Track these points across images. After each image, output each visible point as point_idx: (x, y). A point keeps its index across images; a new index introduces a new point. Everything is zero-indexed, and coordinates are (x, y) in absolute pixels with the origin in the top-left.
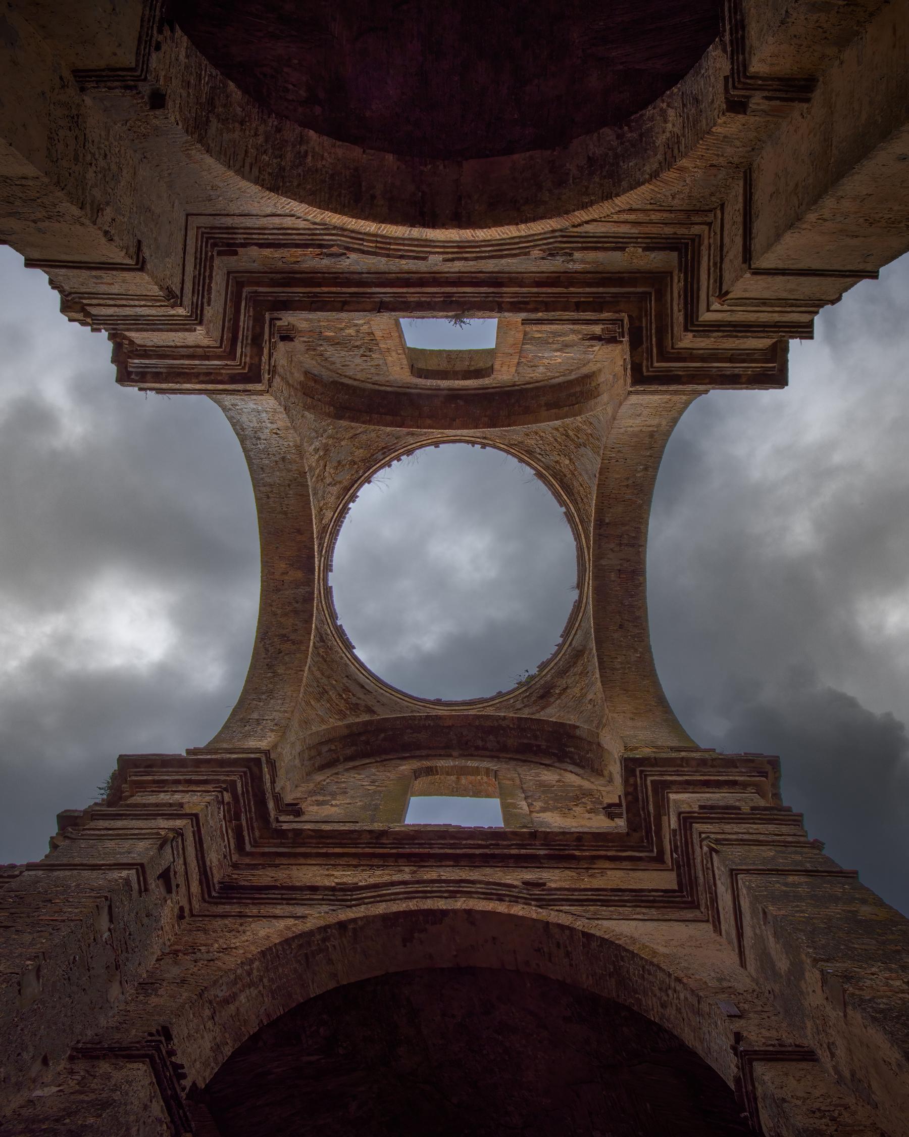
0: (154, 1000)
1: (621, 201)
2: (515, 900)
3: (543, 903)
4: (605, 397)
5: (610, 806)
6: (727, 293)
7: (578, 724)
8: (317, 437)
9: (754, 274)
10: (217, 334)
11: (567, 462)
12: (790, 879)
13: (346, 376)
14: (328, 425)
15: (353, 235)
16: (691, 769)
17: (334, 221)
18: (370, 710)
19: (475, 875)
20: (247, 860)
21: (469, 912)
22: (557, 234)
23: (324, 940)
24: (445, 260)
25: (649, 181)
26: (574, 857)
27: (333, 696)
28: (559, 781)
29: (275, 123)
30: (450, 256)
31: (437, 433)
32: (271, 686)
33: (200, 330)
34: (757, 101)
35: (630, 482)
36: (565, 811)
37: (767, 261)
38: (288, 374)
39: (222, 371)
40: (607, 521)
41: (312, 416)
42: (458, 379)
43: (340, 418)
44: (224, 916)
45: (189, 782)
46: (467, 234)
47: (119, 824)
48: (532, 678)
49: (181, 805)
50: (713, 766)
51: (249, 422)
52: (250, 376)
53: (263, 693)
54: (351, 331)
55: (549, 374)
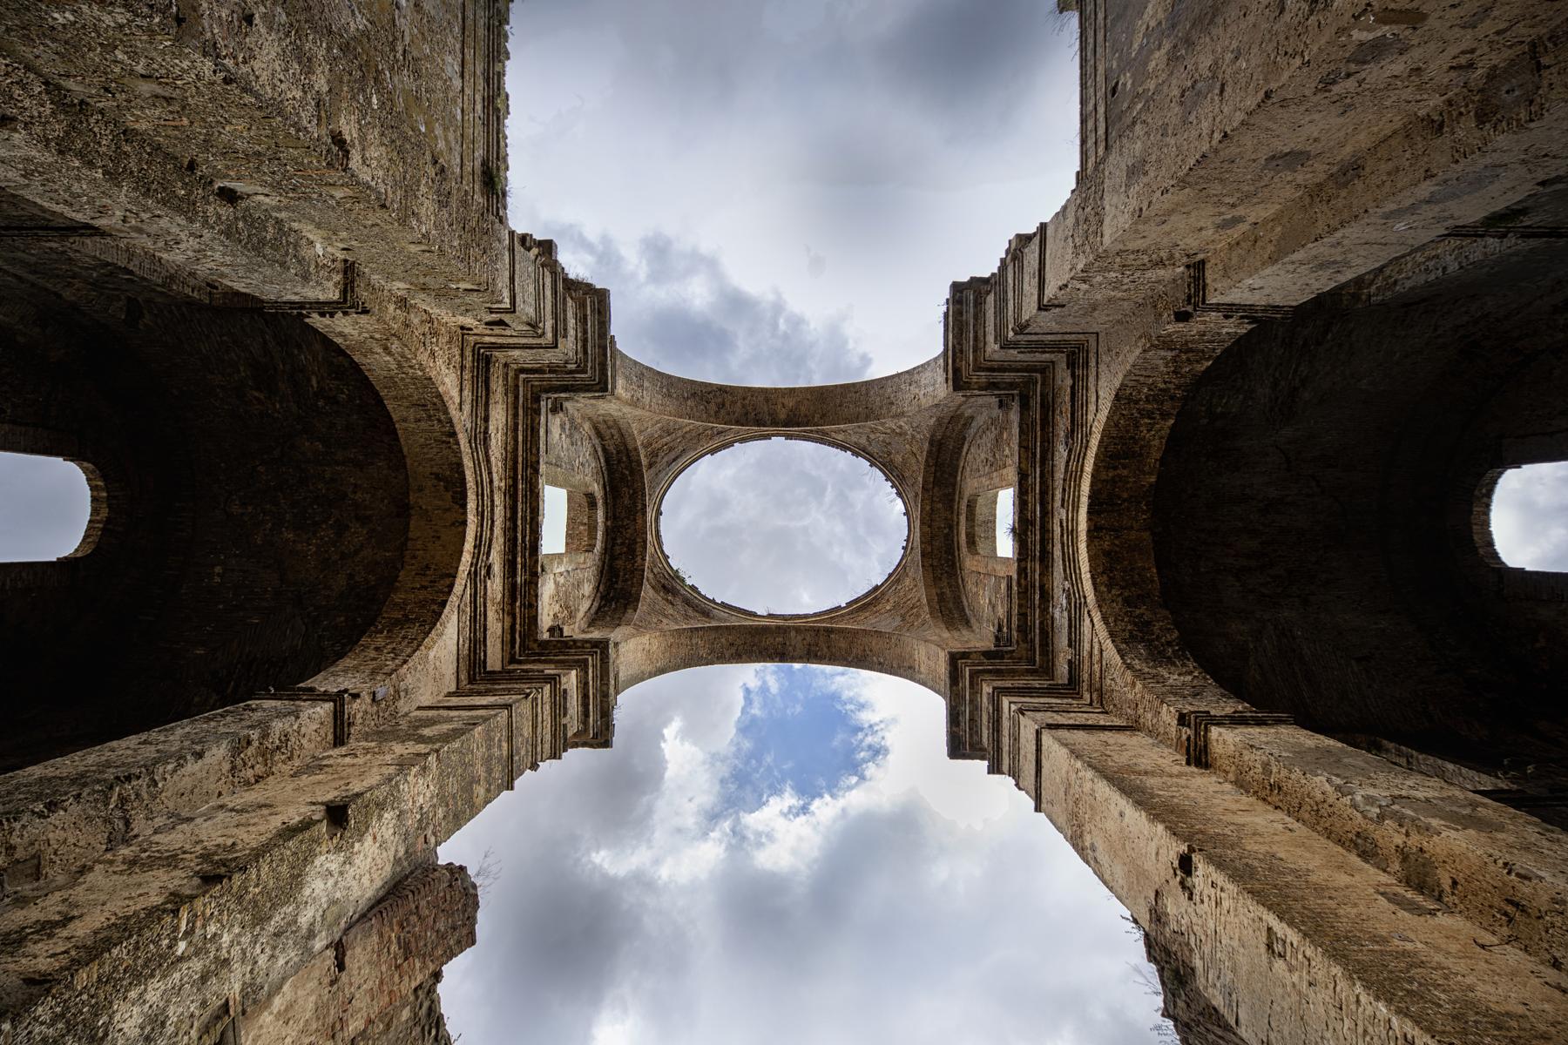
0: (392, 307)
1: (1109, 645)
2: (476, 556)
3: (473, 575)
4: (946, 634)
5: (561, 630)
10: (996, 357)
12: (505, 745)
18: (650, 466)
19: (498, 531)
20: (511, 374)
21: (464, 523)
23: (439, 421)
25: (1124, 662)
26: (513, 599)
31: (917, 514)
33: (997, 347)
34: (1187, 732)
36: (556, 597)
37: (1046, 738)
43: (931, 444)
44: (462, 355)
45: (585, 341)
46: (1083, 537)
47: (548, 293)
48: (683, 580)
49: (565, 336)
51: (926, 378)
52: (958, 382)
54: (1007, 452)
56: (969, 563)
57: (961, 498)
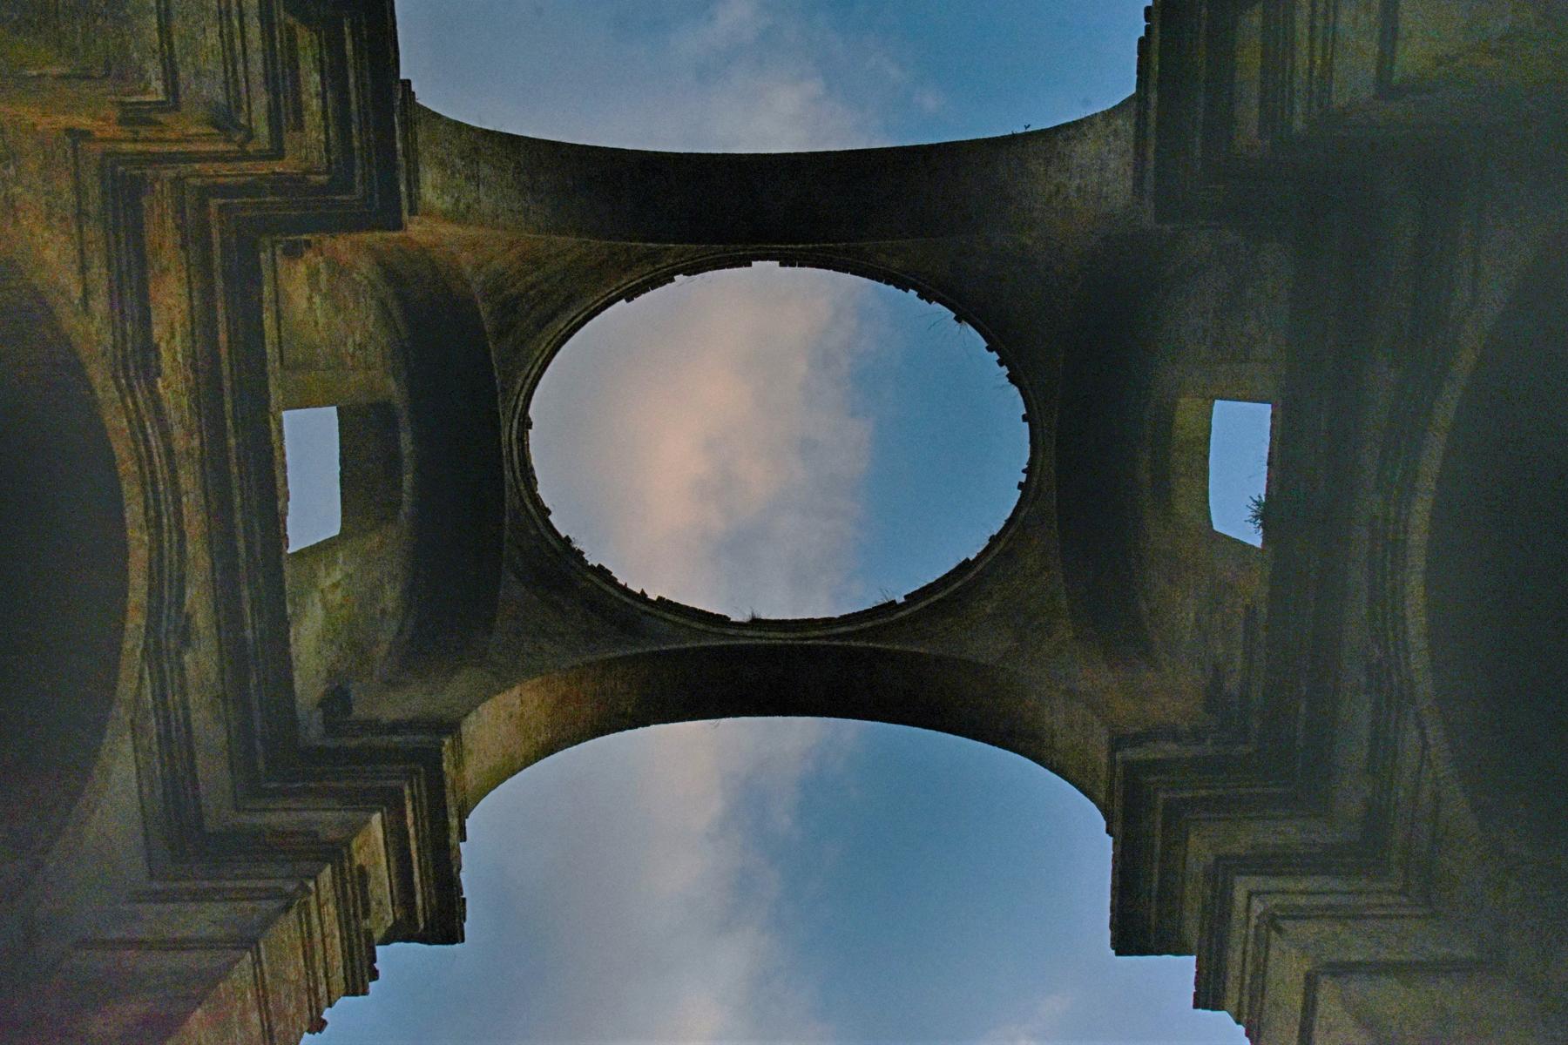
3: (154, 653)
6: (1279, 930)
9: (1308, 976)
12: (255, 1017)
18: (500, 334)
28: (383, 611)
44: (79, 190)
49: (300, 126)
51: (1085, 151)
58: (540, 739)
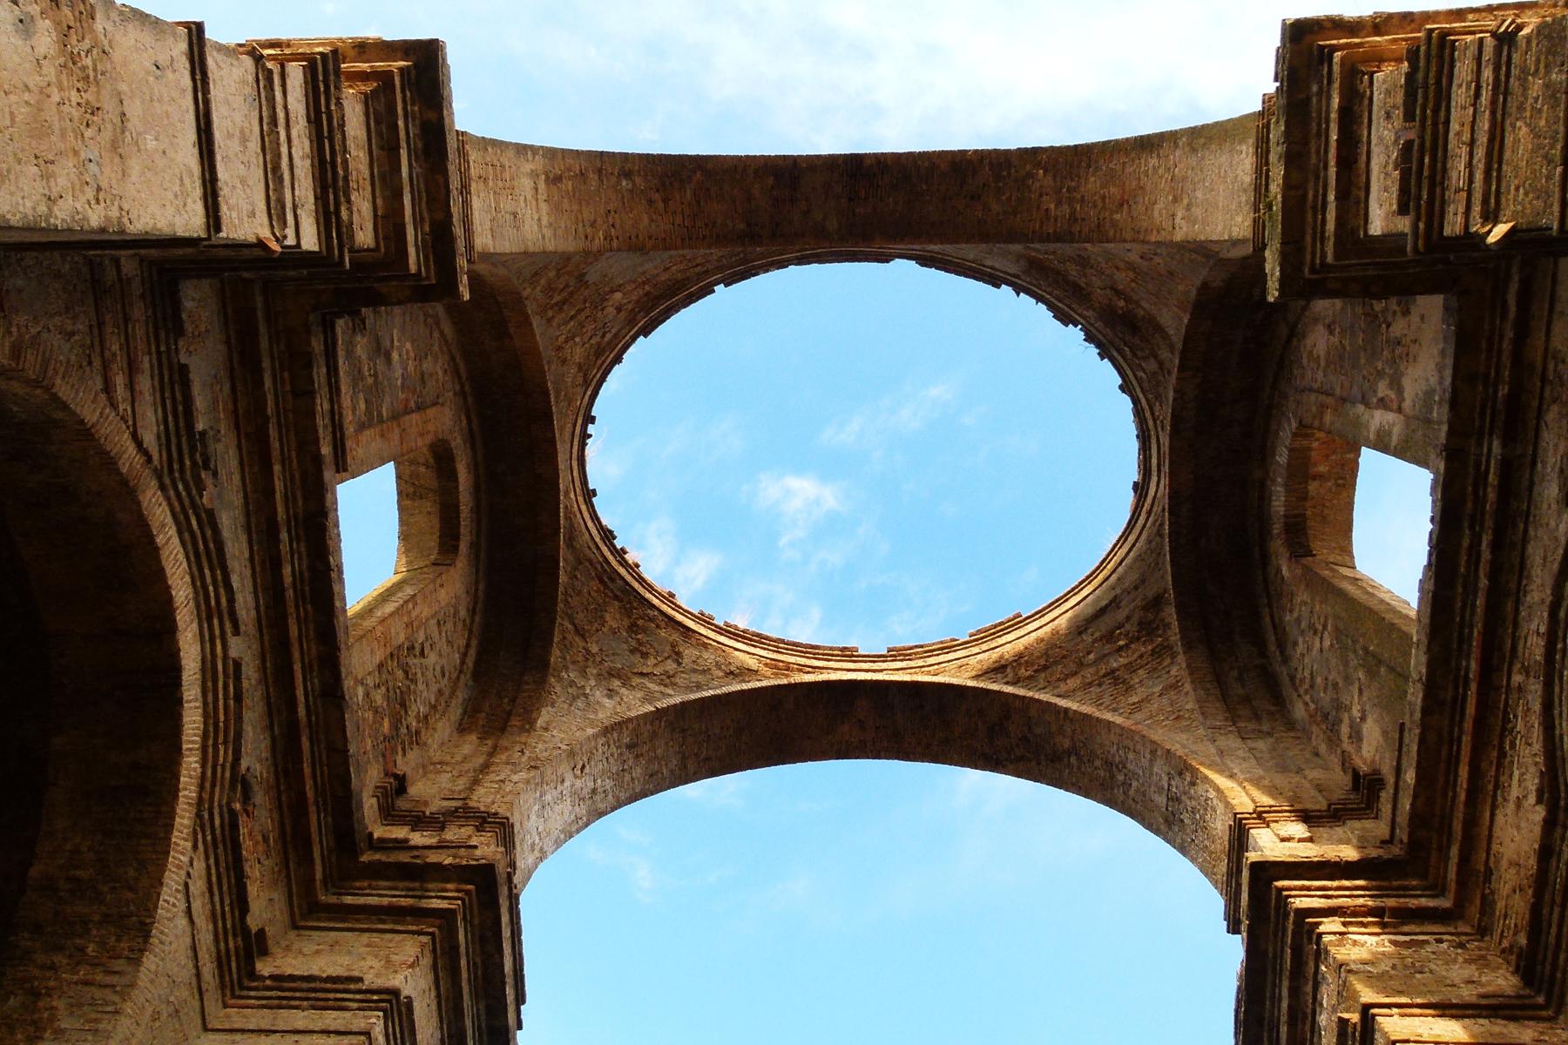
7: (1198, 282)
8: (586, 696)
11: (618, 295)
13: (463, 662)
14: (560, 679)
15: (208, 785)
16: (1311, 184)
17: (186, 822)
20: (1474, 911)
22: (167, 481)
24: (237, 632)
27: (1122, 661)
29: (26, 935)
30: (228, 625)
32: (1098, 763)
35: (657, 197)
38: (467, 766)
39: (476, 922)
40: (742, 226)
41: (544, 711)
42: (457, 488)
50: (1306, 143)
53: (1112, 777)
55: (436, 348)
56: (444, 421)
57: (475, 546)
58: (1153, 161)
